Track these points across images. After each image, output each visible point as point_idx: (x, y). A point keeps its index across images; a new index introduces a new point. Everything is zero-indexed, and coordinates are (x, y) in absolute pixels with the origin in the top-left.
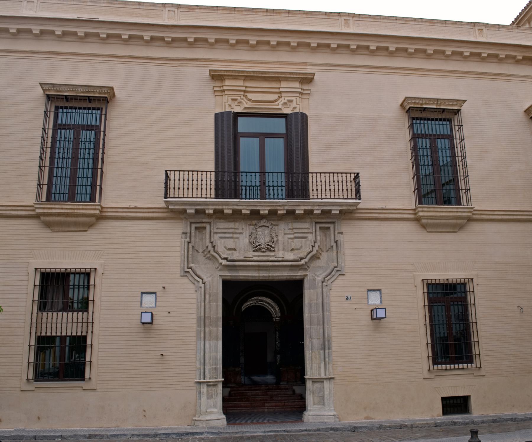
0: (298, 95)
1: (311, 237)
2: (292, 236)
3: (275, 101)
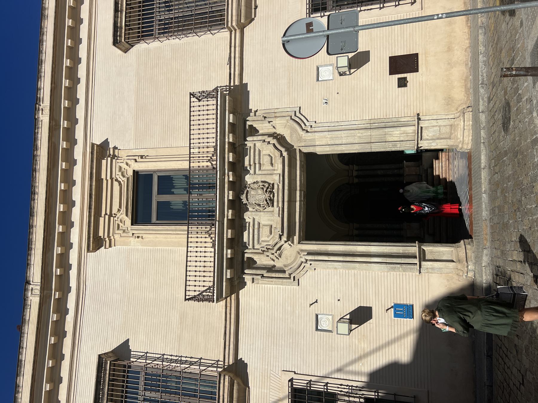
2: (257, 166)
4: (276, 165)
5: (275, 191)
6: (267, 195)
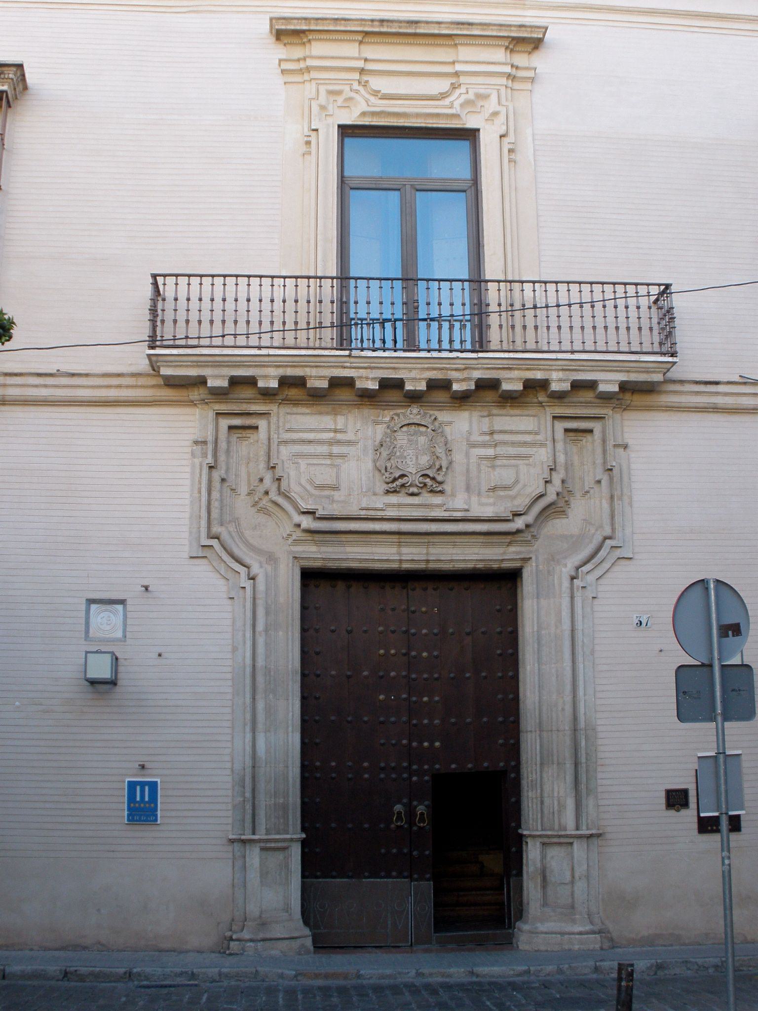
0: (503, 81)
1: (543, 455)
2: (490, 452)
3: (443, 96)
4: (491, 500)
5: (426, 498)
6: (417, 480)
